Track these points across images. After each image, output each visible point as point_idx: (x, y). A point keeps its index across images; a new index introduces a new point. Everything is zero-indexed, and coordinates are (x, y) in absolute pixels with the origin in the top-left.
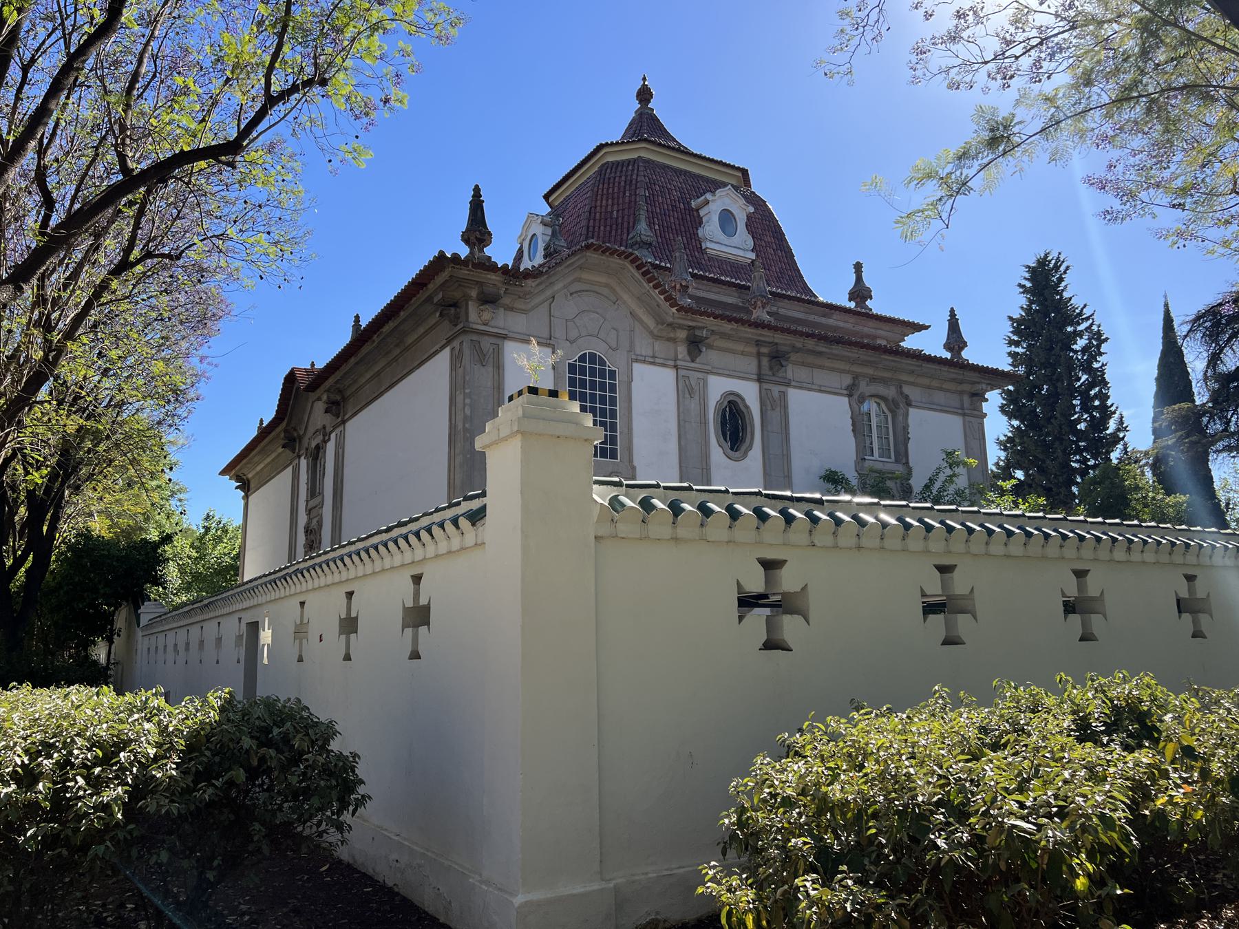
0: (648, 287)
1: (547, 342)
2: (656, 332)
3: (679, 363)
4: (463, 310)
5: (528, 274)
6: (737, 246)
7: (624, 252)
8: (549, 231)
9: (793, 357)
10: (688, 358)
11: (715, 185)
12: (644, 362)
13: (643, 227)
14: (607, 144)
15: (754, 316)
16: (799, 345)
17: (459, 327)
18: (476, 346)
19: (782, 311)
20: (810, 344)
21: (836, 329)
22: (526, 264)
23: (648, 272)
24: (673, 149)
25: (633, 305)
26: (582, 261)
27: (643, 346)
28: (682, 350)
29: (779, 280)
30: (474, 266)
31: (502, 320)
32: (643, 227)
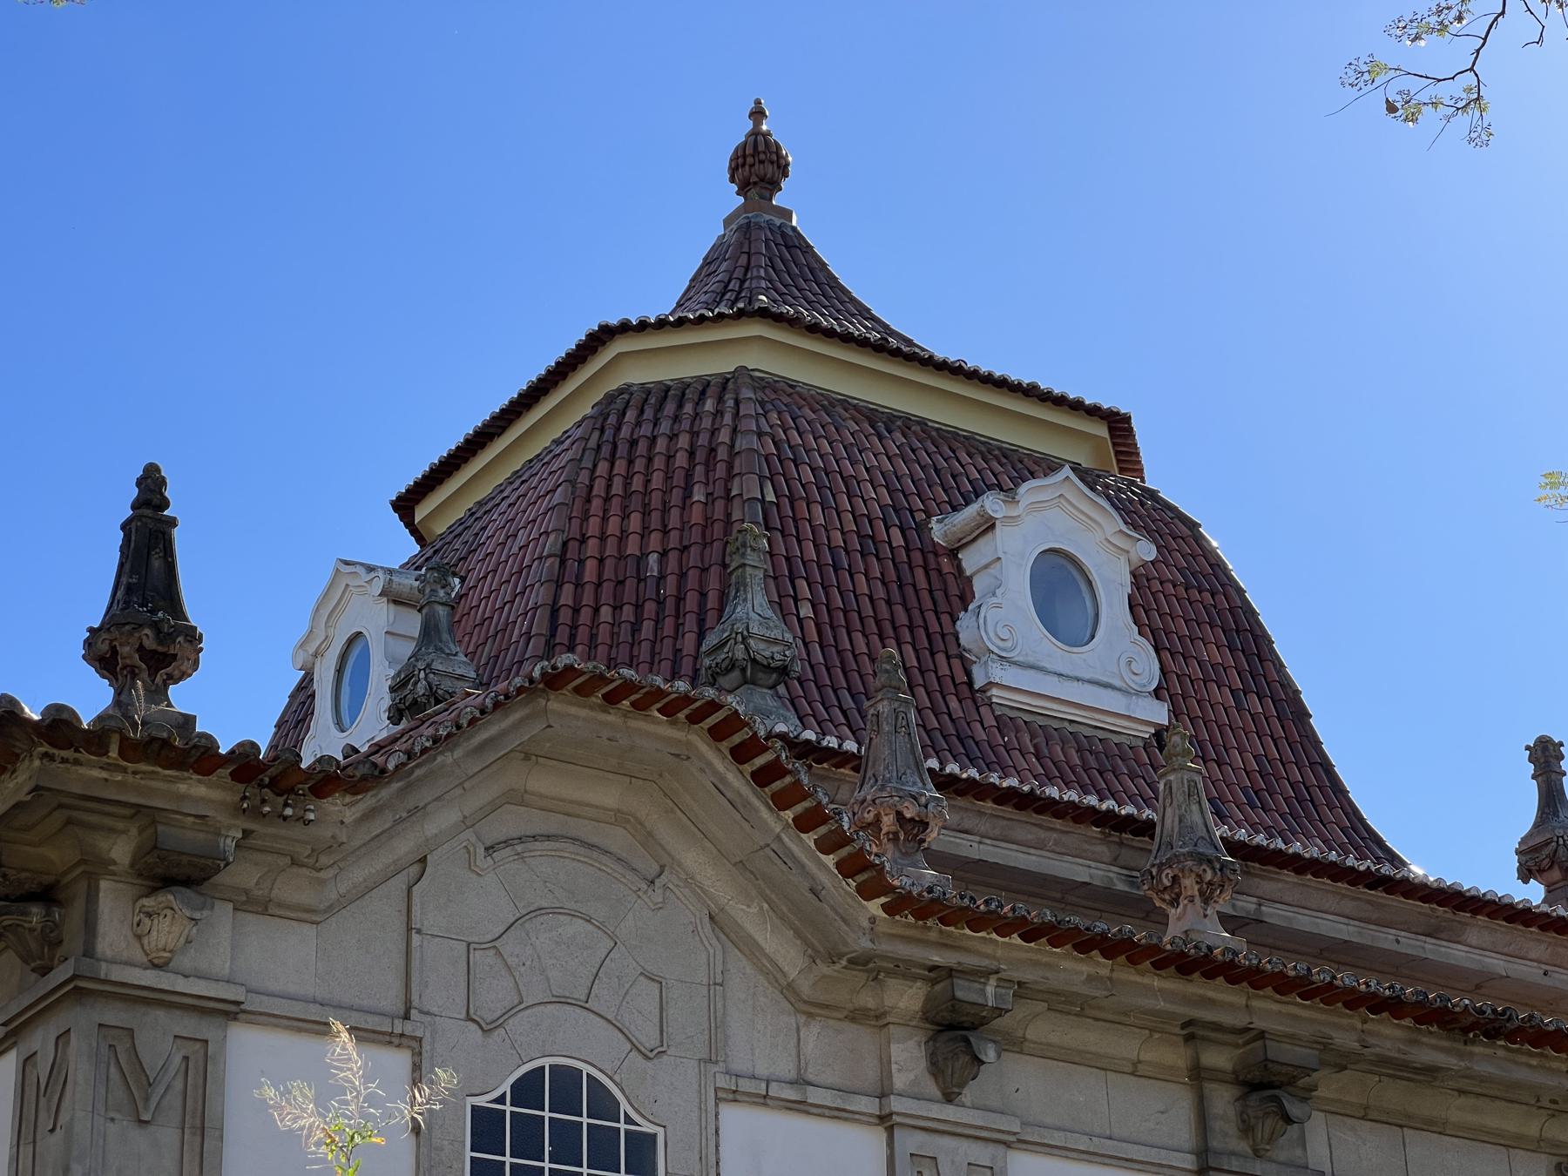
0: (778, 823)
1: (395, 1029)
2: (805, 987)
3: (896, 1104)
4: (78, 907)
5: (330, 780)
6: (1107, 678)
7: (686, 700)
8: (412, 623)
9: (1329, 1086)
10: (932, 1089)
11: (1015, 468)
12: (764, 1100)
13: (755, 614)
14: (625, 328)
15: (1174, 930)
16: (1345, 1040)
17: (61, 974)
18: (119, 1047)
19: (1274, 914)
20: (1389, 1035)
21: (1480, 982)
22: (323, 742)
23: (772, 771)
24: (862, 343)
25: (722, 888)
26: (537, 727)
27: (763, 1039)
28: (908, 1058)
29: (1257, 798)
30: (131, 750)
31: (225, 947)
32: (755, 614)
